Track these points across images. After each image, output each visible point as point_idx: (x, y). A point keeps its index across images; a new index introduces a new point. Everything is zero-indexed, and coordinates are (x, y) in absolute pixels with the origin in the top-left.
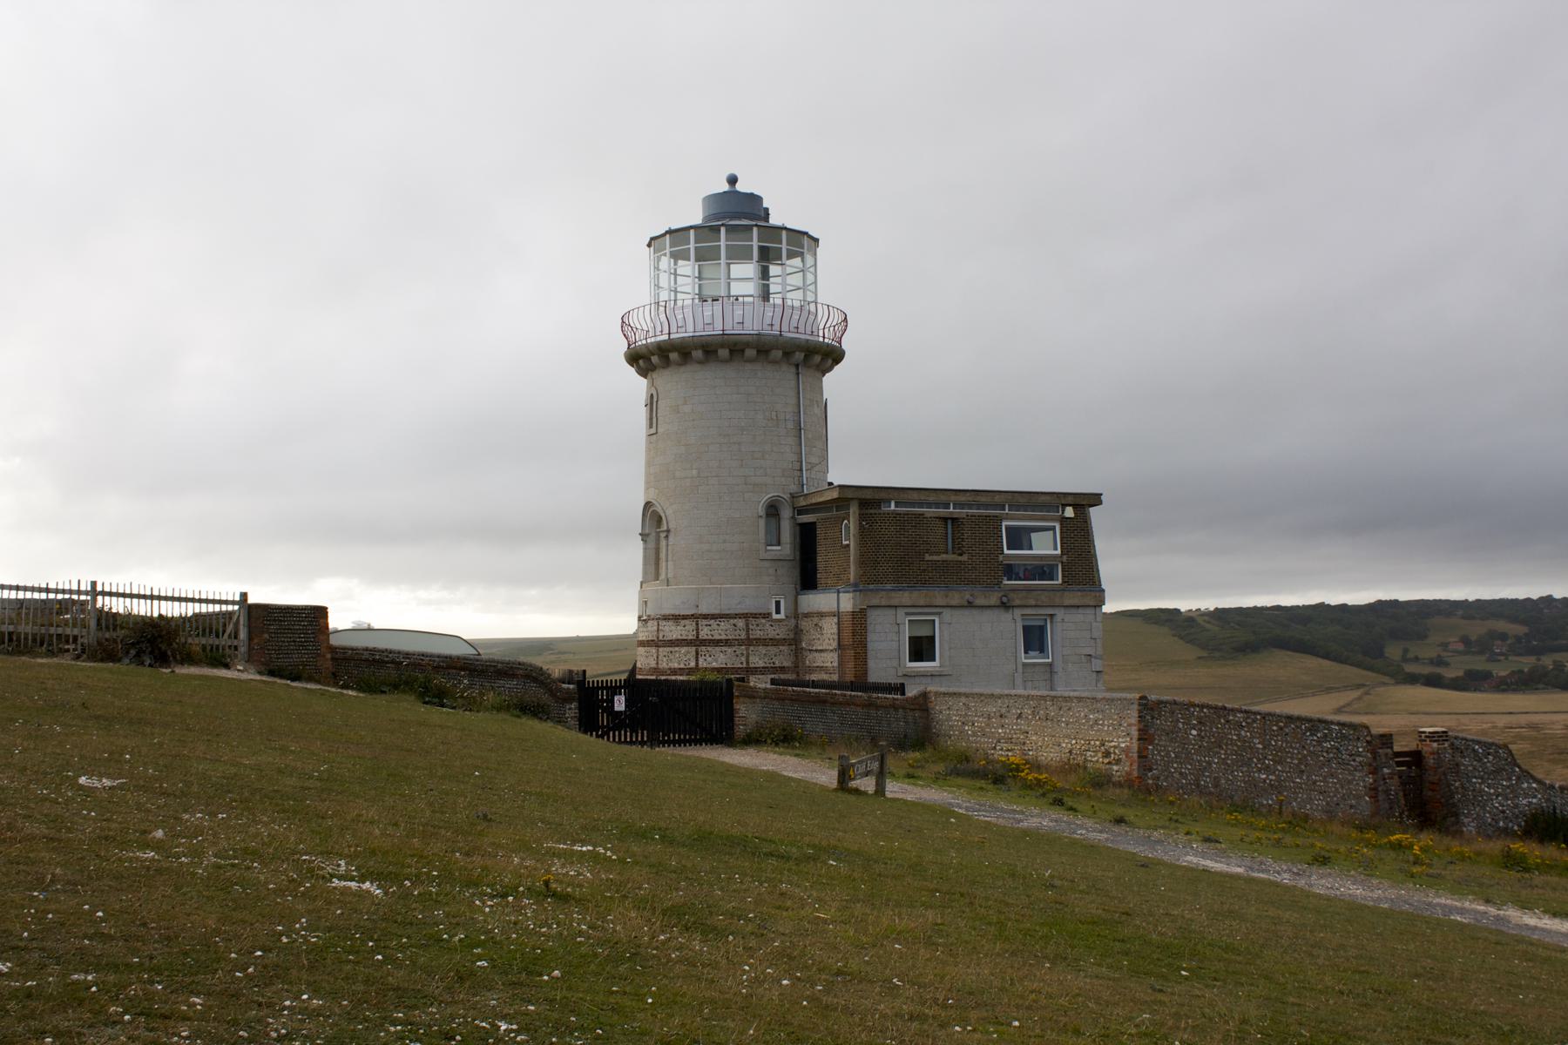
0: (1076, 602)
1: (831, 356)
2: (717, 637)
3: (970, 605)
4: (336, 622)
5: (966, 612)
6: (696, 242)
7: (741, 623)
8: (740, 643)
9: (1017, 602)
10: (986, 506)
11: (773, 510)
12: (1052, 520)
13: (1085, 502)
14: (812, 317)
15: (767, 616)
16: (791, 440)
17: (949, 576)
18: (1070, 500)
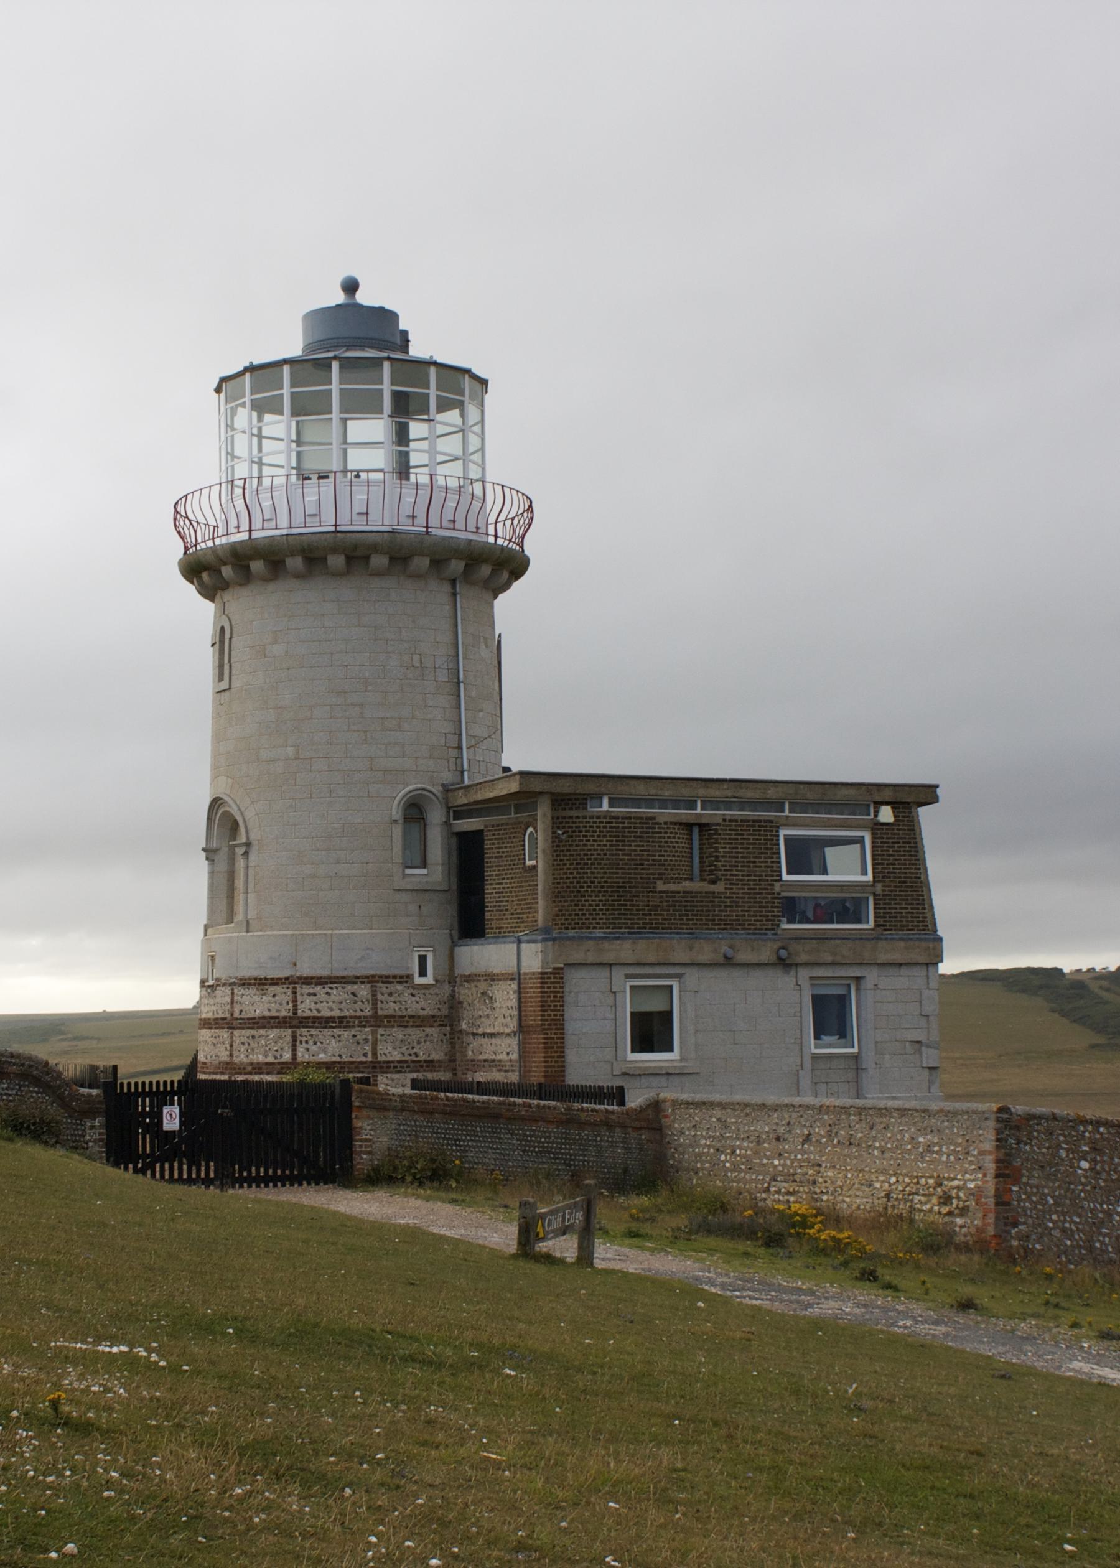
0: (897, 957)
1: (508, 566)
2: (325, 1013)
3: (728, 962)
5: (722, 973)
7: (364, 991)
8: (363, 1022)
9: (803, 958)
10: (754, 805)
12: (858, 827)
13: (912, 798)
14: (476, 505)
17: (694, 916)
18: (887, 795)
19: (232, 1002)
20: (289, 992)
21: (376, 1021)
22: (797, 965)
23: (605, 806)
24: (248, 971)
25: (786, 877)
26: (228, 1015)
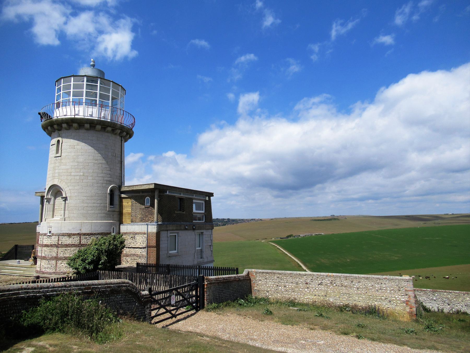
19: (58, 240)
20: (79, 237)
21: (57, 246)
23: (168, 193)
24: (66, 231)
25: (194, 211)
26: (56, 244)
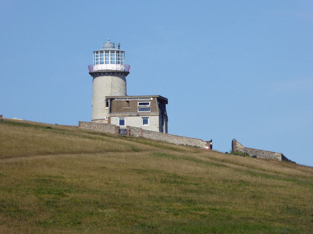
0: (153, 115)
3: (131, 116)
4: (166, 105)
6: (111, 53)
7: (100, 121)
9: (140, 115)
10: (134, 98)
11: (107, 100)
15: (104, 119)
16: (111, 88)
17: (126, 110)
22: (162, 118)
